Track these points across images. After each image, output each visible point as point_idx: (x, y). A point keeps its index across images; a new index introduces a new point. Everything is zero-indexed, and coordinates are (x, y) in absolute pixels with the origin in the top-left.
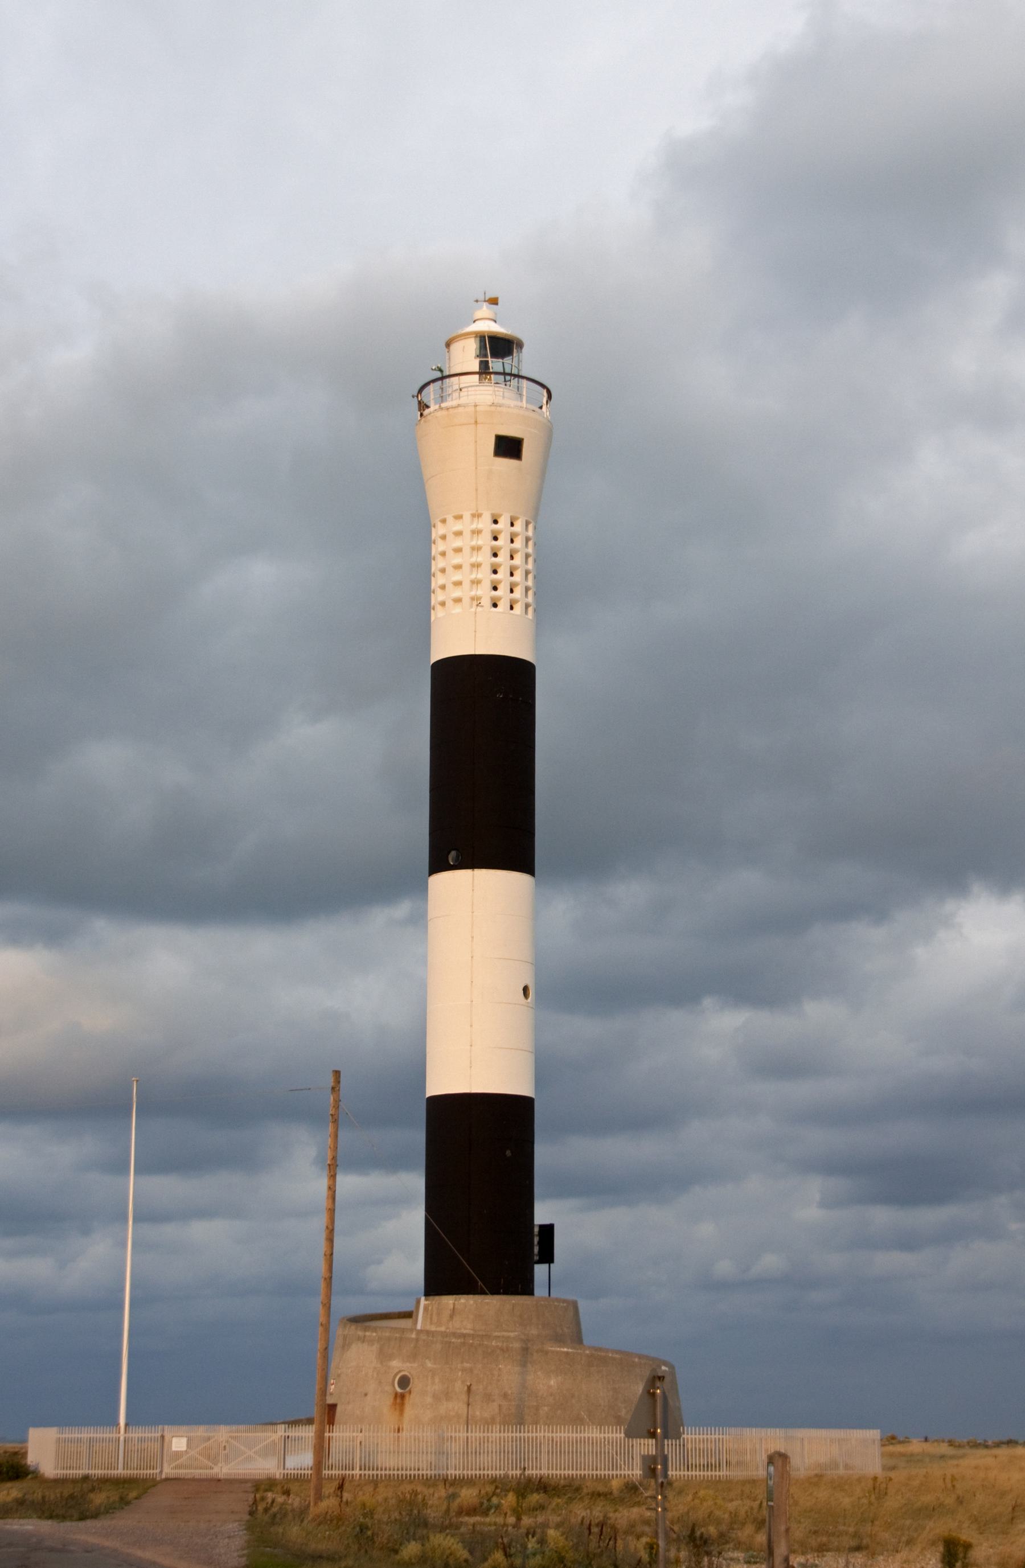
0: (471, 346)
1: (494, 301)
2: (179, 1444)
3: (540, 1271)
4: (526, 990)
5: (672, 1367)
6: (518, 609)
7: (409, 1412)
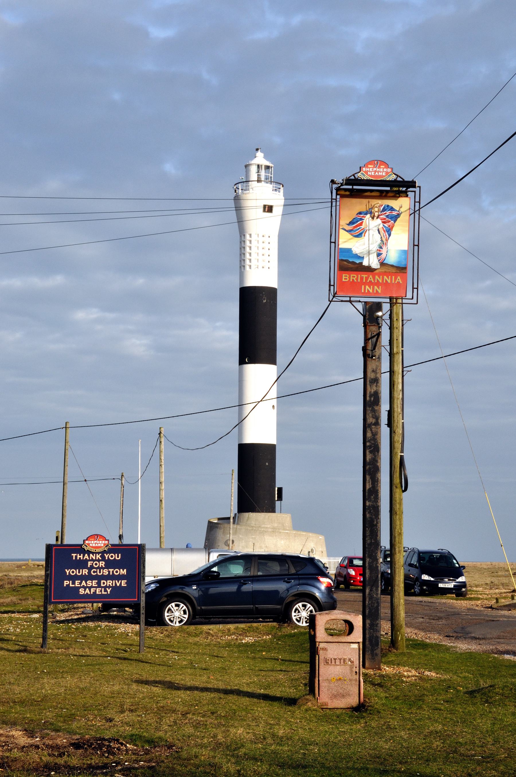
3: (278, 503)
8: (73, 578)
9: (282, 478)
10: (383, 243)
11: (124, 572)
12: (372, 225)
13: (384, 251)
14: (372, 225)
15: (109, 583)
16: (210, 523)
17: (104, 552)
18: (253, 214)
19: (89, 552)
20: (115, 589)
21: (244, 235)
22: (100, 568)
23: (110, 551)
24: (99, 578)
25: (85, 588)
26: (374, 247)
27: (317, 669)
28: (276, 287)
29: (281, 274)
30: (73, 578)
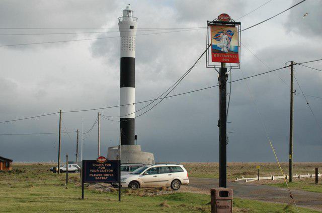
8: (93, 173)
10: (229, 43)
11: (112, 171)
12: (224, 37)
13: (229, 46)
14: (224, 37)
15: (107, 175)
16: (11, 161)
17: (105, 163)
19: (99, 163)
20: (109, 177)
22: (103, 170)
23: (106, 163)
24: (103, 173)
25: (98, 177)
26: (225, 45)
30: (93, 173)
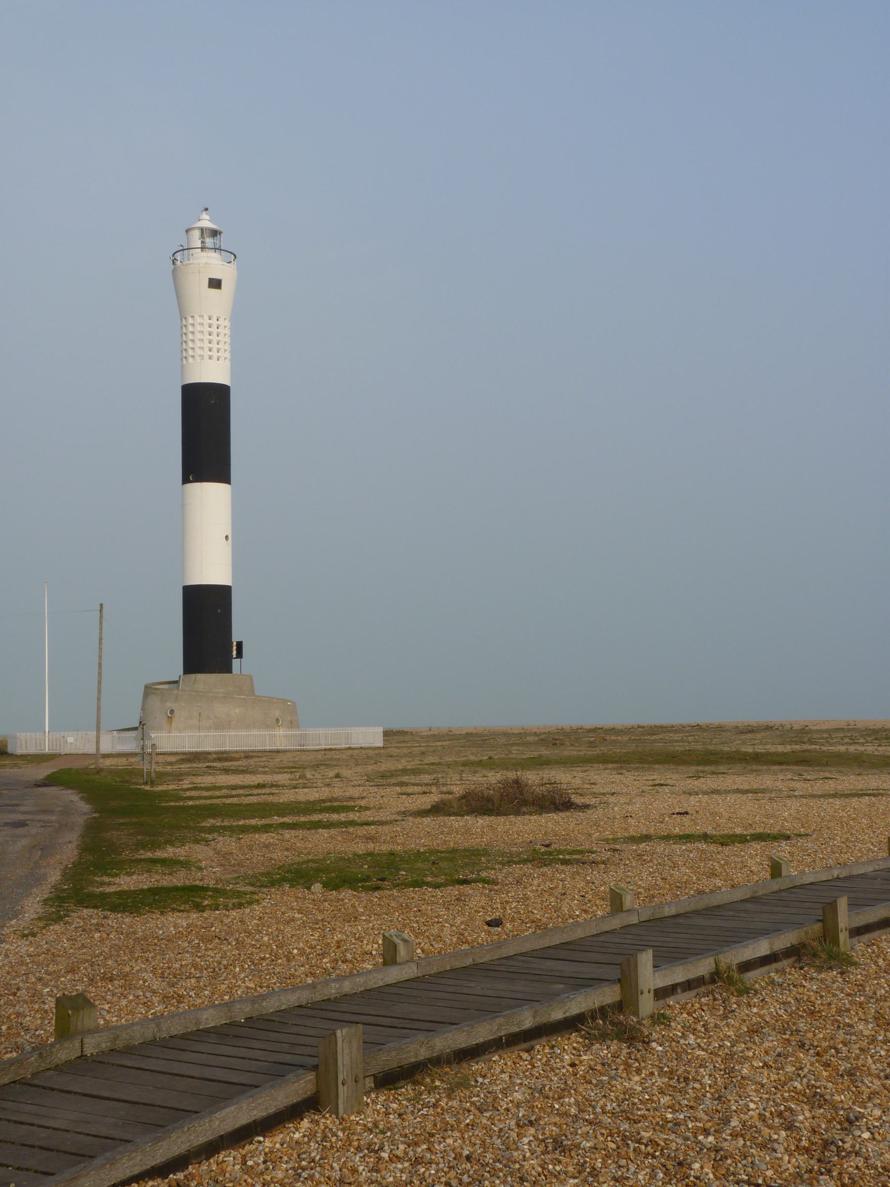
0: (196, 234)
1: (206, 209)
2: (70, 740)
3: (236, 663)
4: (227, 537)
5: (294, 704)
6: (222, 359)
7: (174, 724)
9: (241, 628)
18: (197, 286)
21: (185, 318)
27: (208, 802)
28: (227, 383)
29: (232, 379)
